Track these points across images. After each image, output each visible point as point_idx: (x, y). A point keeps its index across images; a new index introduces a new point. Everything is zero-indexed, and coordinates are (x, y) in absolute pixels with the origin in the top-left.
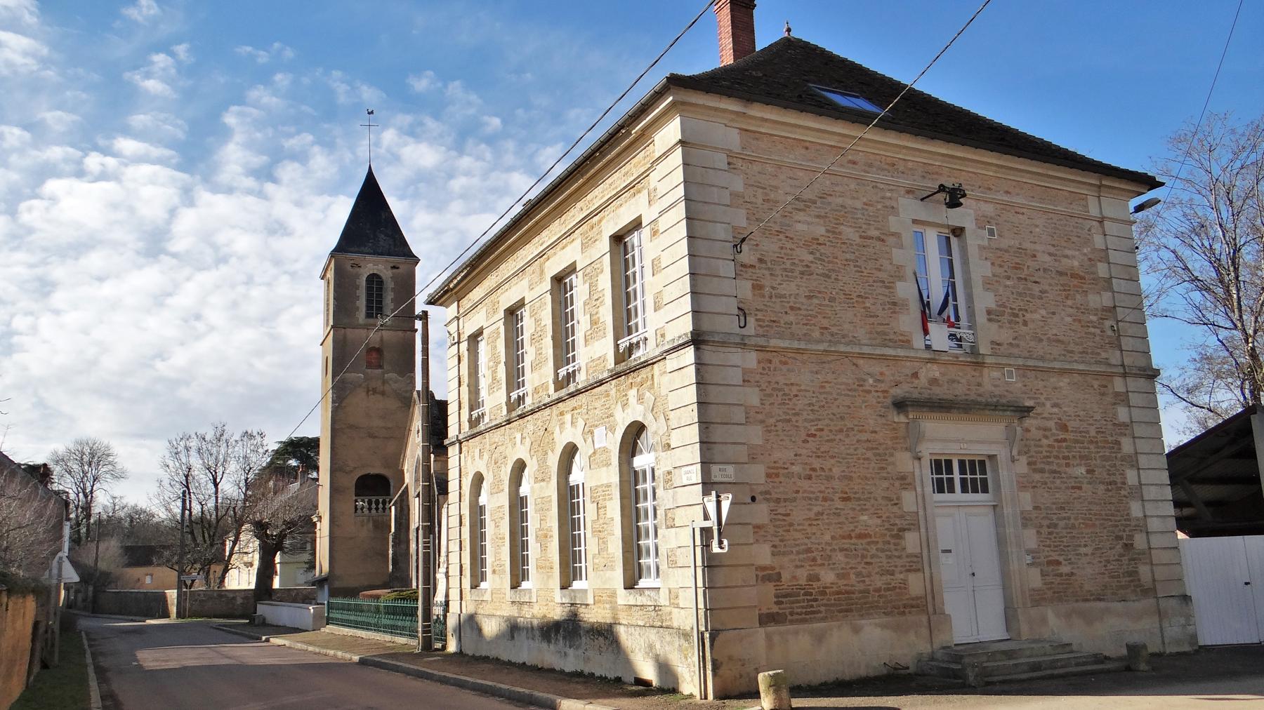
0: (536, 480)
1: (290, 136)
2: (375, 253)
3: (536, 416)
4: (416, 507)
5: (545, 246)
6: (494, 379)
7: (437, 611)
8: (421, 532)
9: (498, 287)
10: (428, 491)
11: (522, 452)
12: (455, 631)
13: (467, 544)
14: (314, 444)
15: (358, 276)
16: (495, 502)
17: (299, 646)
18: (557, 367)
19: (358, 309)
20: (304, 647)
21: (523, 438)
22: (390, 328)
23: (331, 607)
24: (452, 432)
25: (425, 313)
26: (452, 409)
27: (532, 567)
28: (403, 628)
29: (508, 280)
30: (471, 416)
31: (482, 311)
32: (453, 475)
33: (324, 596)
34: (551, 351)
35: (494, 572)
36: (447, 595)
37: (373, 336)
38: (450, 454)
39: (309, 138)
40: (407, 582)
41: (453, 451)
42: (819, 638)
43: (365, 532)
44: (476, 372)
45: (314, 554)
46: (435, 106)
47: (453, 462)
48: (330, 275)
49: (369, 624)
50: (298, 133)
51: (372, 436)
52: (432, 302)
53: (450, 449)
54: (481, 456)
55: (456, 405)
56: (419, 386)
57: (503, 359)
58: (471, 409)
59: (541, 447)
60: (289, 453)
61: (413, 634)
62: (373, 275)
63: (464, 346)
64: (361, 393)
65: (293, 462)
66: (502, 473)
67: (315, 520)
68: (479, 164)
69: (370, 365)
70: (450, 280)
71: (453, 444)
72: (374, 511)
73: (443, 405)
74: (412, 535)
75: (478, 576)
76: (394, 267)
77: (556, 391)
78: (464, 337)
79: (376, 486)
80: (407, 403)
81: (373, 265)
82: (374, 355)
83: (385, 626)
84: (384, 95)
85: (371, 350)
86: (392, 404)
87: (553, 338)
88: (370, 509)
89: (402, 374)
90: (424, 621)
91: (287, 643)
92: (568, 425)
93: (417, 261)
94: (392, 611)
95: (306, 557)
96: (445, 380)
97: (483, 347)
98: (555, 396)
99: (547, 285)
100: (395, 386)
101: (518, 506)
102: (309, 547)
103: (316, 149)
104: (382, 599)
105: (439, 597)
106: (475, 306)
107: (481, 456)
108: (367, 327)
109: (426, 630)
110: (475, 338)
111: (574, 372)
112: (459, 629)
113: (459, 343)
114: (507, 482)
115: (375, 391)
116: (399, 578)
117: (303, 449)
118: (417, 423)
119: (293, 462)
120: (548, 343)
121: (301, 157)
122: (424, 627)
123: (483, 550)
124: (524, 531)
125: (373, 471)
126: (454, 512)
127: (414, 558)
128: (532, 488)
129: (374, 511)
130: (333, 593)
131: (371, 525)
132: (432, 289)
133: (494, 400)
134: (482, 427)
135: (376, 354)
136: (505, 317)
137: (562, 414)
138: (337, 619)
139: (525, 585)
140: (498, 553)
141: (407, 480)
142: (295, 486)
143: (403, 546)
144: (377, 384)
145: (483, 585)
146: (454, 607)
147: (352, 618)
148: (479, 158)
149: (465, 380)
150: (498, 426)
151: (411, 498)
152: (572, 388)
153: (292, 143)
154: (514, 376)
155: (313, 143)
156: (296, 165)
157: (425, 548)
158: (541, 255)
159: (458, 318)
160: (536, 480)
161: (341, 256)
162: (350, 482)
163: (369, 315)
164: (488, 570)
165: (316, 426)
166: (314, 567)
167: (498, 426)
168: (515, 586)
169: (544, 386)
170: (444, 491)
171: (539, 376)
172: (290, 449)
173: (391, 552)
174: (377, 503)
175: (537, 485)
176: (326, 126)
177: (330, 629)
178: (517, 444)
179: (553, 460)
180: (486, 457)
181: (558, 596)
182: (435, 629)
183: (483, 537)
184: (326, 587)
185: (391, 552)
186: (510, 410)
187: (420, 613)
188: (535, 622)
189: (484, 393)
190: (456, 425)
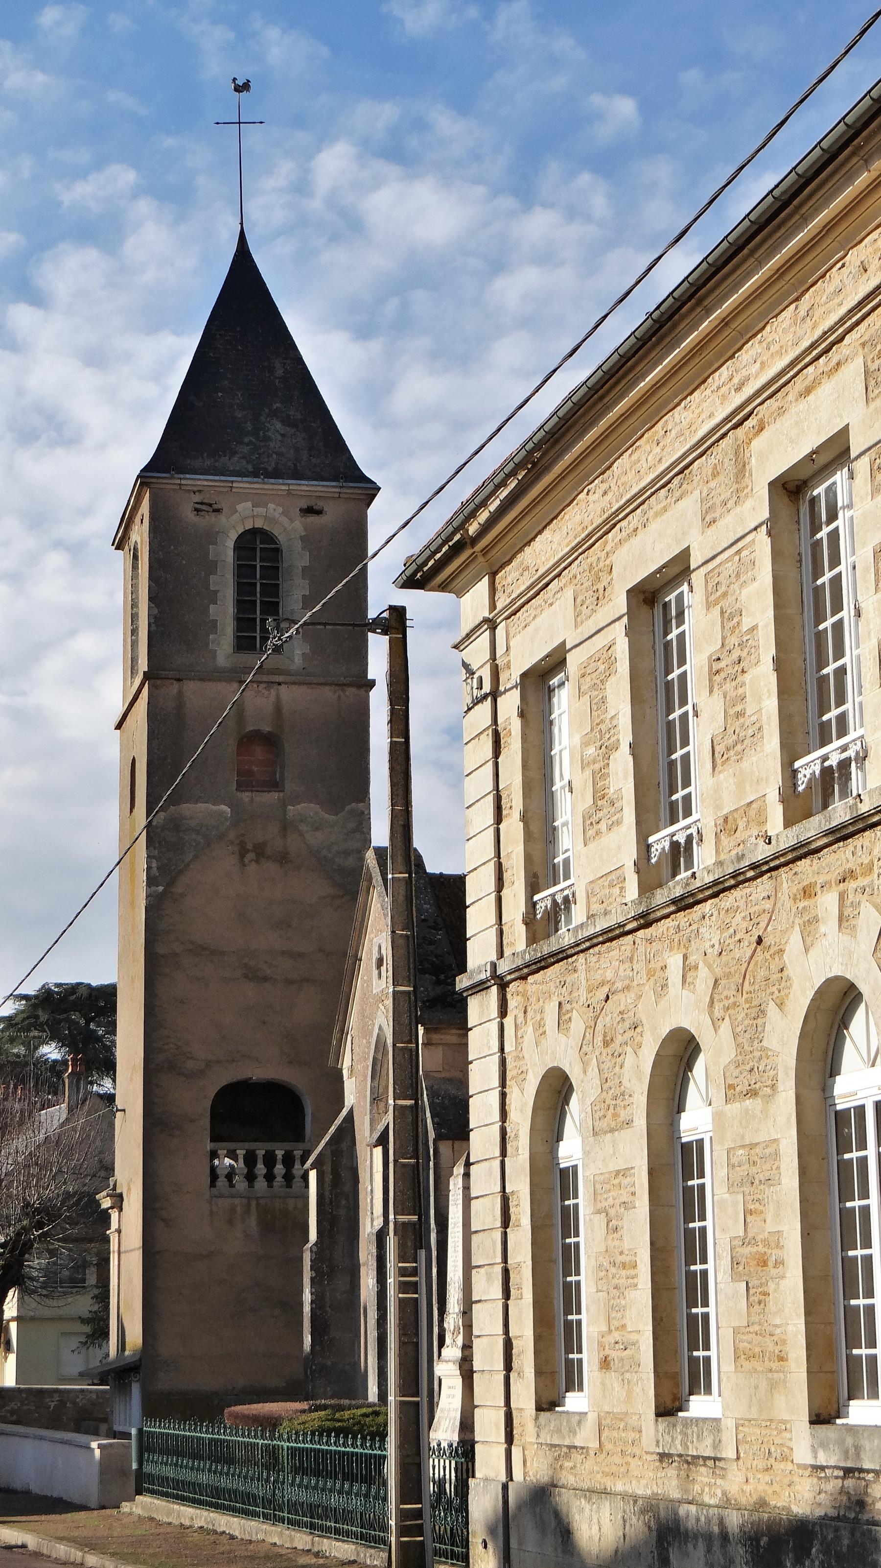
0: (731, 1093)
1: (80, 173)
2: (258, 472)
3: (728, 900)
4: (373, 1170)
5: (749, 390)
6: (599, 795)
7: (440, 1468)
8: (391, 1242)
9: (610, 524)
10: (409, 1119)
11: (685, 1010)
12: (492, 1531)
13: (522, 1212)
14: (101, 1001)
16: (606, 1155)
17: (62, 1550)
18: (790, 754)
19: (214, 624)
20: (76, 1555)
21: (688, 969)
22: (302, 679)
23: (146, 1444)
24: (479, 953)
25: (398, 614)
26: (478, 890)
27: (719, 1353)
28: (345, 1516)
29: (638, 501)
30: (532, 905)
31: (566, 608)
32: (482, 1076)
33: (130, 1415)
34: (771, 705)
35: (605, 1363)
36: (467, 1425)
37: (259, 703)
38: (473, 1019)
39: (126, 177)
40: (353, 1383)
41: (481, 1010)
44: (547, 778)
45: (103, 1297)
46: (451, 72)
47: (481, 1039)
48: (140, 535)
49: (249, 1498)
50: (99, 164)
51: (254, 976)
52: (415, 579)
53: (473, 1005)
54: (562, 1023)
55: (488, 874)
56: (380, 833)
57: (626, 736)
58: (533, 886)
59: (744, 988)
60: (40, 1027)
61: (370, 1533)
63: (510, 703)
64: (224, 860)
65: (51, 1052)
66: (627, 1073)
67: (106, 1203)
68: (574, 231)
69: (246, 782)
70: (469, 511)
71: (480, 987)
72: (261, 1184)
73: (450, 892)
74: (367, 1253)
75: (557, 1378)
76: (310, 511)
77: (788, 823)
78: (511, 677)
79: (267, 1115)
80: (349, 888)
81: (253, 505)
82: (259, 752)
83: (293, 1507)
84: (325, 51)
85: (249, 740)
86: (312, 888)
87: (779, 664)
88: (251, 1178)
89: (334, 804)
90: (403, 1498)
91: (31, 1540)
92: (829, 926)
93: (371, 491)
94: (312, 1465)
95: (84, 1304)
96: (459, 831)
97: (565, 703)
98: (787, 839)
99: (757, 506)
100: (316, 839)
101: (675, 1167)
102: (92, 1278)
103: (144, 207)
104: (284, 1428)
105: (444, 1431)
106: (540, 586)
107: (562, 1023)
108: (235, 675)
109: (410, 1523)
110: (542, 678)
111: (844, 765)
112: (504, 1527)
113: (495, 694)
114: (640, 1100)
115: (260, 852)
116: (329, 1372)
117: (76, 1014)
118: (378, 937)
119: (51, 1052)
120: (763, 680)
121: (100, 231)
122: (403, 1515)
123: (571, 1298)
124: (695, 1246)
125: (258, 1073)
126: (487, 1184)
127: (372, 1315)
128: (718, 1117)
129: (261, 1184)
130: (154, 1408)
131: (253, 1222)
132: (410, 544)
133: (600, 861)
134: (565, 937)
135: (261, 751)
136: (631, 612)
137: (808, 892)
138: (164, 1481)
139: (699, 1406)
140: (616, 1309)
141: (350, 1099)
142: (55, 1116)
143: (341, 1283)
145: (574, 1402)
146: (489, 1461)
147: (204, 1478)
148: (574, 213)
149: (515, 801)
150: (612, 935)
151: (362, 1149)
152: (840, 812)
153: (83, 194)
154: (661, 787)
155: (136, 193)
156: (92, 254)
157: (404, 1287)
158: (738, 419)
159: (491, 624)
160: (731, 1093)
161: (170, 483)
162: (196, 1101)
164: (588, 1357)
165: (104, 955)
166: (106, 1335)
167: (612, 935)
168: (668, 1408)
169: (753, 811)
170: (455, 1124)
171: (736, 786)
172: (43, 1016)
174: (270, 1160)
175: (735, 1108)
176: (170, 142)
177: (144, 1505)
178: (672, 985)
179: (784, 1033)
180: (578, 1024)
181: (803, 1443)
182: (437, 1522)
183: (570, 1259)
184: (136, 1390)
185: (307, 1297)
186: (646, 888)
187: (391, 1470)
188: (734, 1520)
189: (568, 842)
190: (486, 938)
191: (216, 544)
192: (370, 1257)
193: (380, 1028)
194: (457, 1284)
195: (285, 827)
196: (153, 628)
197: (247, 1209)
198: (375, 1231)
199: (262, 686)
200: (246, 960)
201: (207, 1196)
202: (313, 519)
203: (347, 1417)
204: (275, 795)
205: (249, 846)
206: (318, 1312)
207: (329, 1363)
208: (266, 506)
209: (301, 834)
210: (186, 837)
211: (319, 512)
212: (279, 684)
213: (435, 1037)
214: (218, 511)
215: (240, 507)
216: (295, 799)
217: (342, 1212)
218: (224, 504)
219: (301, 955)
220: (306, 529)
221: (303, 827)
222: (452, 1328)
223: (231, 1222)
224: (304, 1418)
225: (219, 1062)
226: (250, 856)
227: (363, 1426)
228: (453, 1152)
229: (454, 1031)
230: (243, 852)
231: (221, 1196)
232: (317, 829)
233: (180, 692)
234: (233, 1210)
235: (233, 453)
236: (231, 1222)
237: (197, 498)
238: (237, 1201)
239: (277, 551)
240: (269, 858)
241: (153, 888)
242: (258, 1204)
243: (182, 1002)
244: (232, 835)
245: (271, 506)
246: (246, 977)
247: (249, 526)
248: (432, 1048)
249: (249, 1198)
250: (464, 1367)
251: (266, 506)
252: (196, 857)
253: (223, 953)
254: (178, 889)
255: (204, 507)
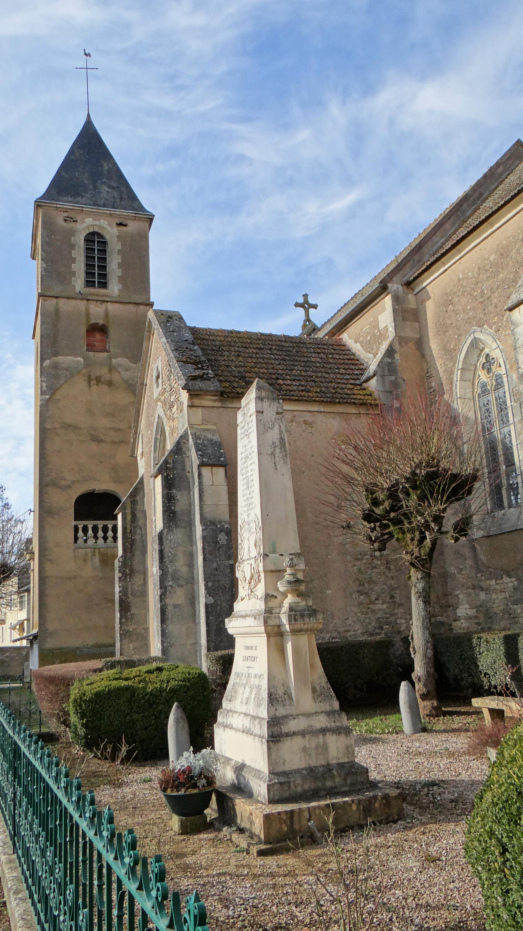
15: (72, 233)
37: (97, 312)
42: (104, 920)
43: (90, 570)
62: (93, 234)
64: (81, 384)
76: (120, 224)
108: (81, 297)
115: (98, 380)
129: (101, 541)
131: (97, 560)
141: (141, 471)
143: (138, 579)
144: (103, 372)
162: (66, 502)
163: (89, 284)
173: (117, 589)
185: (117, 589)
191: (74, 236)
192: (154, 553)
193: (159, 417)
194: (253, 525)
195: (111, 369)
196: (44, 273)
197: (94, 555)
198: (157, 534)
199: (98, 303)
200: (92, 432)
201: (73, 548)
202: (123, 228)
203: (134, 674)
204: (106, 354)
205: (93, 377)
206: (124, 598)
207: (131, 629)
208: (99, 220)
209: (119, 373)
210: (61, 372)
211: (126, 225)
212: (107, 302)
213: (197, 402)
214: (76, 221)
215: (86, 220)
216: (116, 357)
217: (137, 538)
218: (78, 217)
219: (119, 430)
220: (119, 232)
221: (120, 369)
222: (248, 577)
223: (85, 561)
224: (94, 677)
225: (78, 481)
226: (94, 382)
227: (147, 684)
228: (212, 474)
229: (209, 397)
230: (90, 380)
231: (80, 548)
232: (127, 370)
233: (57, 304)
234: (86, 554)
235: (83, 197)
236: (85, 561)
237: (65, 214)
238: (88, 550)
239: (105, 243)
240: (103, 383)
241: (44, 396)
242: (99, 552)
243: (59, 452)
244: (84, 371)
245: (102, 221)
246: (92, 440)
247: (91, 231)
248: (194, 409)
249: (95, 548)
250: (271, 622)
251: (99, 220)
252: (66, 382)
253: (80, 428)
254: (57, 396)
255: (68, 219)
